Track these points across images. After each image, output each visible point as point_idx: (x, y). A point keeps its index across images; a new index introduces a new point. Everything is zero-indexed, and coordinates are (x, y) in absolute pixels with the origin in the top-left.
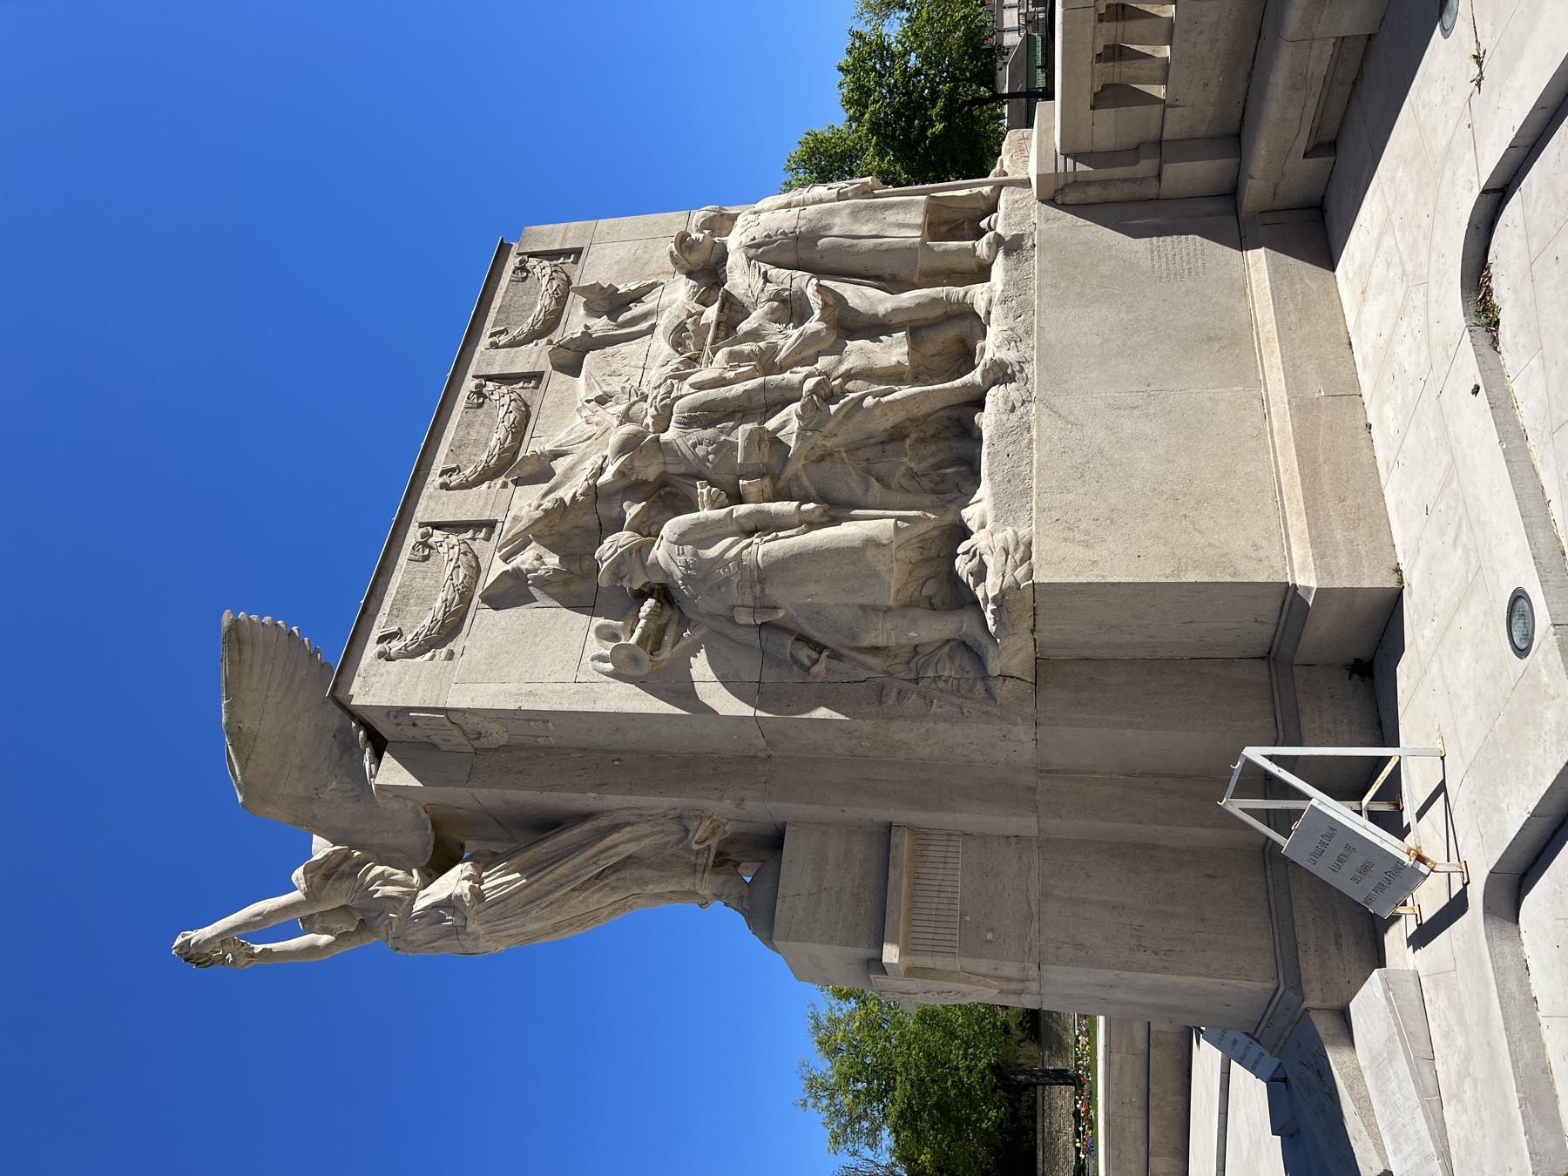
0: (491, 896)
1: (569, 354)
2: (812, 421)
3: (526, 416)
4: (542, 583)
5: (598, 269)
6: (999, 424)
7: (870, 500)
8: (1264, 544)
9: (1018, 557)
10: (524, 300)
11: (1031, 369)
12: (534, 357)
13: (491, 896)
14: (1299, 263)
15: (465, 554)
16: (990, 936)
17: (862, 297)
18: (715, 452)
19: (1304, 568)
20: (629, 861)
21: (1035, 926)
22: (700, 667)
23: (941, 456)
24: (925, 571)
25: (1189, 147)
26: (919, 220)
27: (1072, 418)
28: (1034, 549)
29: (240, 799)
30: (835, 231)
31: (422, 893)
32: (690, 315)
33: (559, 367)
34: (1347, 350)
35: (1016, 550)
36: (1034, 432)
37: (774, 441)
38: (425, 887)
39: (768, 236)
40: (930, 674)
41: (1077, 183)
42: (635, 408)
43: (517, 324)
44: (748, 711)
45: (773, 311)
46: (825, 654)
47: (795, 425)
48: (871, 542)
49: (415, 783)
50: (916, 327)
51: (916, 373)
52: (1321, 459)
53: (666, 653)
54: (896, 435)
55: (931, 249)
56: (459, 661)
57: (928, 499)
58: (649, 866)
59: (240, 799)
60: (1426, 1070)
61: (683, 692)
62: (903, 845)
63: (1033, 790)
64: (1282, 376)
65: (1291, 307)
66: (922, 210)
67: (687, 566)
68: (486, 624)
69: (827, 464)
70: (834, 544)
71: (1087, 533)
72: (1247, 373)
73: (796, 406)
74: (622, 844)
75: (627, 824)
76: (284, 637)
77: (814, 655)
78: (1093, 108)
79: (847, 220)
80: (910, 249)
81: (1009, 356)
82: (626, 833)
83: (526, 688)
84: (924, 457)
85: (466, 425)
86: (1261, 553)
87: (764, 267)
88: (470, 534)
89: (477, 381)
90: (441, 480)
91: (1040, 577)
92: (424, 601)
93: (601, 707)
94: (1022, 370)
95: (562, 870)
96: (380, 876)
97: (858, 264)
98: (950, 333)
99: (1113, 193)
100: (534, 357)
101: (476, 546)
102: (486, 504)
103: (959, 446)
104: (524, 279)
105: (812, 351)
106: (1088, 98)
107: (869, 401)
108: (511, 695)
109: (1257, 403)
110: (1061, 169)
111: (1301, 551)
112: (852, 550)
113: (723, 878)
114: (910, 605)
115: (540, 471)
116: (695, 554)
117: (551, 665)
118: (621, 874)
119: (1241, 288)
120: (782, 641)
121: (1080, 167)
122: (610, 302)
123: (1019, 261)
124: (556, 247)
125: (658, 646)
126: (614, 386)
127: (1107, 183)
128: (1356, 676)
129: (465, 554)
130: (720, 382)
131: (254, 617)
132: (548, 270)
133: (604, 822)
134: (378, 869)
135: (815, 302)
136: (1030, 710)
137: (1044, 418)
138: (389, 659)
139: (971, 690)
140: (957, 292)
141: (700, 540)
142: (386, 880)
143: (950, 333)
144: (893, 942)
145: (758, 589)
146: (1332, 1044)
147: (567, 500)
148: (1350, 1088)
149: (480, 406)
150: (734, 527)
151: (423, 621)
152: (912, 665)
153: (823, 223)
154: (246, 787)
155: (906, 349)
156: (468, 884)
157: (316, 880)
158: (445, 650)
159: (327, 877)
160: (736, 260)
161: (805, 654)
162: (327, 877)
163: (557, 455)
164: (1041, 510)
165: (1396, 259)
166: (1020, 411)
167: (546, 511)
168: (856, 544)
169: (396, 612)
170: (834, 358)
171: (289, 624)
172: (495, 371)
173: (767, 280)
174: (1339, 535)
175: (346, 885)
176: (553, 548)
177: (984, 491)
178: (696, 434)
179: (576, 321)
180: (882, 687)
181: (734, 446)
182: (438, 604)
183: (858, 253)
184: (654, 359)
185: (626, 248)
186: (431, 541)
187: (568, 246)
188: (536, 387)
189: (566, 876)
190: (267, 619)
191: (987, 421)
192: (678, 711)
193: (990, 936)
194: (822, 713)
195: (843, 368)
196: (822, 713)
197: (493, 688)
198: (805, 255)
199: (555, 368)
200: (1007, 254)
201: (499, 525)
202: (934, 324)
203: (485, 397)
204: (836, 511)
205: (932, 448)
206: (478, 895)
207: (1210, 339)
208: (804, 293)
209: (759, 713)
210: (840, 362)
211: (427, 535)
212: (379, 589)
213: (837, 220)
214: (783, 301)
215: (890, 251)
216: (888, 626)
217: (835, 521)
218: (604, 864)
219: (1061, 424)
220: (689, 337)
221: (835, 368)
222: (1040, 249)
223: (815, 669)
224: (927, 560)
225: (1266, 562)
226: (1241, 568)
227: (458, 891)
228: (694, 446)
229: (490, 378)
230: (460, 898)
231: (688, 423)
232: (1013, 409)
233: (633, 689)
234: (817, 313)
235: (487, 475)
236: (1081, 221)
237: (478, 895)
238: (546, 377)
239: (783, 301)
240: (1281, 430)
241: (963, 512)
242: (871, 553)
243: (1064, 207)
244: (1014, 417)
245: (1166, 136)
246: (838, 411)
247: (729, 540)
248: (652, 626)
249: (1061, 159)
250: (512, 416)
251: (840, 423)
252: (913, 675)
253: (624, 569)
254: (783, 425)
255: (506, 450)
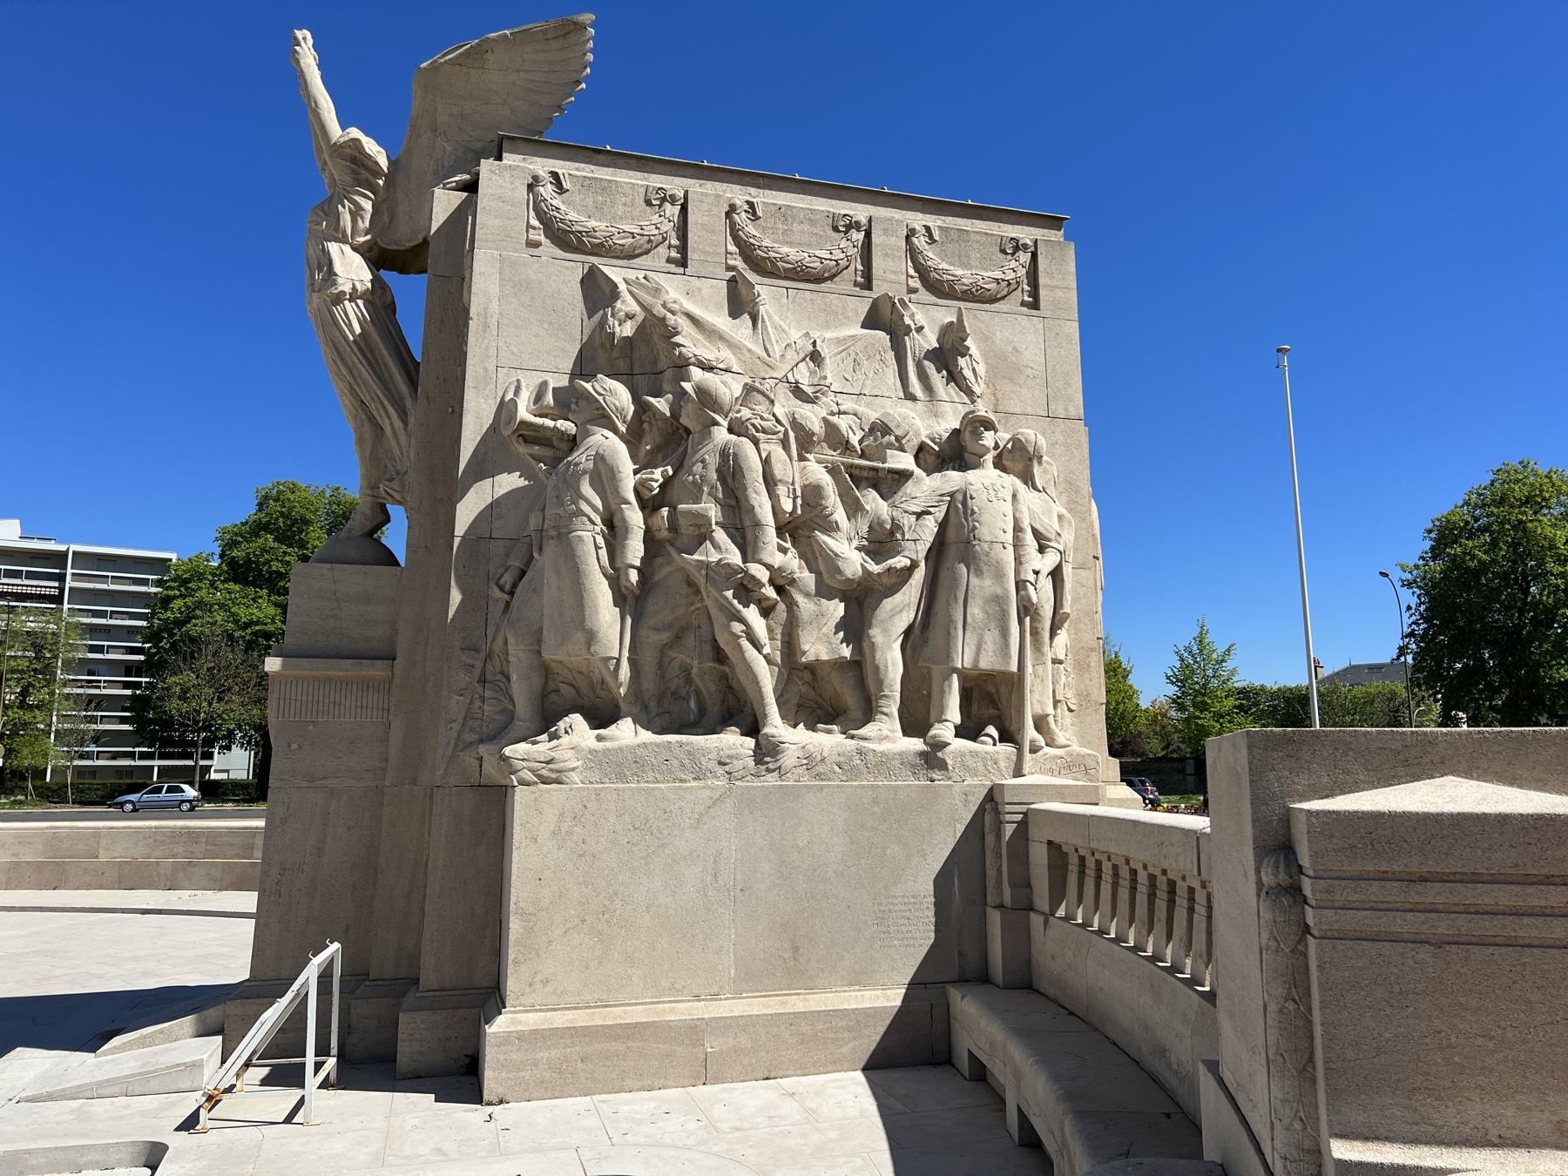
0: (337, 311)
1: (886, 311)
2: (723, 573)
3: (818, 279)
4: (603, 322)
5: (997, 335)
6: (705, 752)
7: (644, 633)
8: (549, 989)
9: (544, 772)
10: (975, 255)
11: (771, 780)
12: (892, 273)
13: (337, 311)
14: (878, 1038)
15: (650, 241)
16: (294, 746)
17: (899, 612)
18: (694, 482)
19: (514, 1022)
20: (378, 429)
21: (306, 784)
22: (509, 482)
23: (706, 696)
24: (583, 686)
25: (1019, 938)
26: (984, 664)
27: (705, 818)
28: (553, 786)
29: (424, 65)
30: (974, 581)
31: (347, 248)
32: (898, 439)
33: (875, 307)
34: (761, 1075)
35: (551, 770)
36: (694, 784)
37: (703, 535)
38: (355, 249)
39: (973, 513)
40: (488, 693)
41: (999, 824)
42: (760, 397)
43: (943, 255)
44: (461, 528)
45: (881, 524)
46: (507, 597)
47: (714, 557)
48: (591, 637)
49: (434, 228)
50: (860, 669)
51: (791, 664)
52: (630, 1044)
53: (522, 449)
54: (719, 656)
55: (948, 677)
56: (525, 254)
57: (649, 685)
58: (374, 447)
59: (424, 65)
60: (117, 1089)
61: (483, 467)
62: (377, 671)
63: (414, 782)
64: (736, 1014)
65: (820, 1027)
66: (998, 667)
67: (577, 464)
68: (567, 272)
69: (684, 590)
70: (587, 601)
71: (569, 833)
72: (750, 979)
73: (735, 557)
74: (390, 421)
75: (405, 424)
76: (574, 77)
77: (507, 587)
78: (1050, 843)
79: (987, 592)
80: (948, 657)
81: (789, 759)
82: (398, 424)
83: (493, 322)
84: (703, 680)
85: (811, 217)
86: (539, 986)
87: (940, 513)
88: (675, 242)
89: (864, 220)
90: (738, 203)
91: (521, 796)
92: (598, 211)
93: (469, 395)
94: (769, 771)
95: (366, 374)
96: (359, 208)
97: (939, 606)
98: (850, 698)
99: (989, 860)
100: (892, 273)
101: (662, 251)
102: (707, 253)
103: (714, 711)
104: (1003, 251)
105: (822, 568)
106: (1057, 839)
107: (737, 627)
108: (486, 309)
109: (714, 989)
110: (1009, 808)
111: (531, 1021)
112: (583, 619)
113: (368, 512)
114: (546, 671)
115: (740, 303)
116: (585, 472)
117: (517, 346)
118: (366, 422)
119: (859, 979)
120: (520, 555)
121: (1009, 830)
122: (948, 355)
123: (913, 766)
124: (1042, 281)
125: (527, 440)
126: (830, 369)
127: (998, 854)
128: (467, 1061)
129: (650, 241)
130: (770, 482)
131: (591, 44)
132: (1010, 276)
133: (409, 403)
134: (368, 206)
135: (900, 562)
136: (452, 781)
137: (708, 793)
138: (530, 187)
139: (472, 729)
140: (893, 706)
141: (600, 476)
142: (356, 212)
143: (850, 698)
144: (284, 666)
145: (553, 533)
146: (198, 1021)
147: (678, 339)
148: (161, 1032)
149: (836, 229)
150: (613, 506)
151: (571, 212)
152: (499, 677)
153: (985, 568)
154: (435, 67)
155: (825, 657)
156: (347, 288)
157: (348, 151)
158: (542, 238)
159: (354, 160)
160: (953, 479)
161: (507, 579)
162: (354, 160)
163: (754, 319)
164: (597, 793)
165: (746, 1125)
166: (720, 770)
167: (664, 319)
168: (588, 624)
169: (587, 184)
170: (812, 587)
171: (587, 79)
172: (875, 239)
173: (919, 515)
174: (543, 1055)
175: (348, 178)
176: (640, 329)
177: (647, 736)
178: (713, 461)
179: (927, 320)
180: (477, 651)
181: (697, 500)
182: (592, 223)
183: (948, 605)
184: (867, 405)
185: (1031, 360)
186: (667, 206)
187: (1042, 292)
188: (856, 284)
189: (360, 375)
190: (590, 57)
191: (733, 741)
192: (462, 466)
193: (294, 746)
194: (456, 597)
195: (799, 598)
196: (456, 597)
197: (495, 290)
198: (952, 551)
199: (875, 300)
200: (922, 754)
201: (681, 270)
202: (861, 683)
203: (846, 233)
204: (628, 601)
205: (713, 687)
206: (338, 299)
207: (796, 949)
208: (899, 553)
209: (457, 541)
210: (807, 595)
211: (673, 200)
212: (621, 162)
213: (988, 582)
214: (892, 533)
215: (949, 636)
216: (521, 655)
217: (620, 599)
218: (372, 407)
219: (700, 808)
220: (876, 440)
221: (801, 591)
222: (927, 787)
223: (496, 590)
224: (593, 688)
225: (528, 990)
226: (523, 968)
227: (340, 281)
228: (703, 461)
229: (868, 234)
230: (334, 283)
231: (724, 454)
232: (721, 763)
233: (488, 421)
234: (875, 568)
235: (746, 250)
236: (960, 828)
237: (338, 299)
238: (866, 293)
239: (892, 533)
240: (672, 1011)
241: (577, 719)
242: (580, 636)
243: (981, 811)
244: (713, 765)
245: (1032, 914)
246: (726, 598)
247: (599, 504)
248: (549, 434)
249: (1023, 808)
250: (817, 264)
251: (717, 601)
252: (489, 676)
253: (582, 403)
254: (716, 547)
255: (774, 265)
